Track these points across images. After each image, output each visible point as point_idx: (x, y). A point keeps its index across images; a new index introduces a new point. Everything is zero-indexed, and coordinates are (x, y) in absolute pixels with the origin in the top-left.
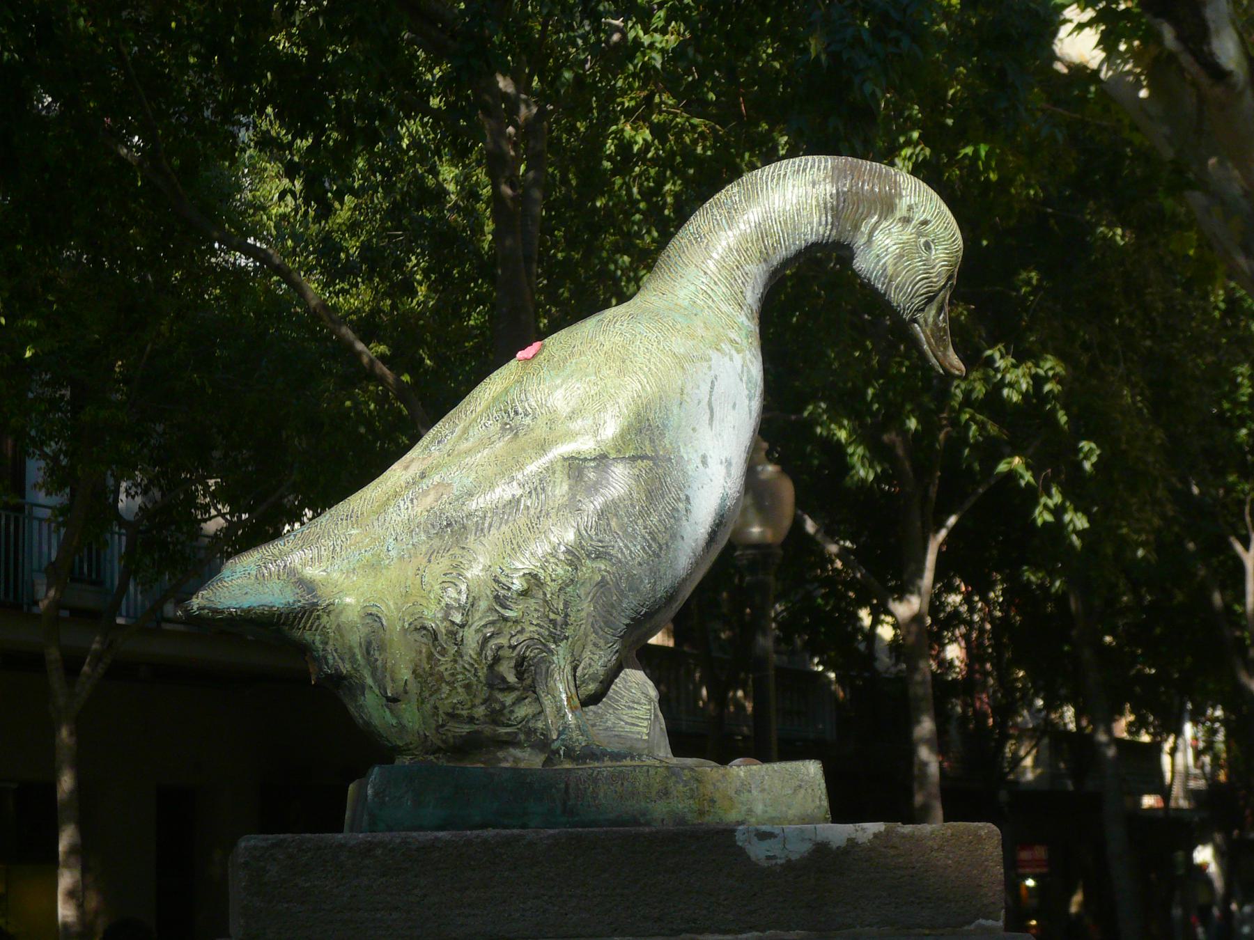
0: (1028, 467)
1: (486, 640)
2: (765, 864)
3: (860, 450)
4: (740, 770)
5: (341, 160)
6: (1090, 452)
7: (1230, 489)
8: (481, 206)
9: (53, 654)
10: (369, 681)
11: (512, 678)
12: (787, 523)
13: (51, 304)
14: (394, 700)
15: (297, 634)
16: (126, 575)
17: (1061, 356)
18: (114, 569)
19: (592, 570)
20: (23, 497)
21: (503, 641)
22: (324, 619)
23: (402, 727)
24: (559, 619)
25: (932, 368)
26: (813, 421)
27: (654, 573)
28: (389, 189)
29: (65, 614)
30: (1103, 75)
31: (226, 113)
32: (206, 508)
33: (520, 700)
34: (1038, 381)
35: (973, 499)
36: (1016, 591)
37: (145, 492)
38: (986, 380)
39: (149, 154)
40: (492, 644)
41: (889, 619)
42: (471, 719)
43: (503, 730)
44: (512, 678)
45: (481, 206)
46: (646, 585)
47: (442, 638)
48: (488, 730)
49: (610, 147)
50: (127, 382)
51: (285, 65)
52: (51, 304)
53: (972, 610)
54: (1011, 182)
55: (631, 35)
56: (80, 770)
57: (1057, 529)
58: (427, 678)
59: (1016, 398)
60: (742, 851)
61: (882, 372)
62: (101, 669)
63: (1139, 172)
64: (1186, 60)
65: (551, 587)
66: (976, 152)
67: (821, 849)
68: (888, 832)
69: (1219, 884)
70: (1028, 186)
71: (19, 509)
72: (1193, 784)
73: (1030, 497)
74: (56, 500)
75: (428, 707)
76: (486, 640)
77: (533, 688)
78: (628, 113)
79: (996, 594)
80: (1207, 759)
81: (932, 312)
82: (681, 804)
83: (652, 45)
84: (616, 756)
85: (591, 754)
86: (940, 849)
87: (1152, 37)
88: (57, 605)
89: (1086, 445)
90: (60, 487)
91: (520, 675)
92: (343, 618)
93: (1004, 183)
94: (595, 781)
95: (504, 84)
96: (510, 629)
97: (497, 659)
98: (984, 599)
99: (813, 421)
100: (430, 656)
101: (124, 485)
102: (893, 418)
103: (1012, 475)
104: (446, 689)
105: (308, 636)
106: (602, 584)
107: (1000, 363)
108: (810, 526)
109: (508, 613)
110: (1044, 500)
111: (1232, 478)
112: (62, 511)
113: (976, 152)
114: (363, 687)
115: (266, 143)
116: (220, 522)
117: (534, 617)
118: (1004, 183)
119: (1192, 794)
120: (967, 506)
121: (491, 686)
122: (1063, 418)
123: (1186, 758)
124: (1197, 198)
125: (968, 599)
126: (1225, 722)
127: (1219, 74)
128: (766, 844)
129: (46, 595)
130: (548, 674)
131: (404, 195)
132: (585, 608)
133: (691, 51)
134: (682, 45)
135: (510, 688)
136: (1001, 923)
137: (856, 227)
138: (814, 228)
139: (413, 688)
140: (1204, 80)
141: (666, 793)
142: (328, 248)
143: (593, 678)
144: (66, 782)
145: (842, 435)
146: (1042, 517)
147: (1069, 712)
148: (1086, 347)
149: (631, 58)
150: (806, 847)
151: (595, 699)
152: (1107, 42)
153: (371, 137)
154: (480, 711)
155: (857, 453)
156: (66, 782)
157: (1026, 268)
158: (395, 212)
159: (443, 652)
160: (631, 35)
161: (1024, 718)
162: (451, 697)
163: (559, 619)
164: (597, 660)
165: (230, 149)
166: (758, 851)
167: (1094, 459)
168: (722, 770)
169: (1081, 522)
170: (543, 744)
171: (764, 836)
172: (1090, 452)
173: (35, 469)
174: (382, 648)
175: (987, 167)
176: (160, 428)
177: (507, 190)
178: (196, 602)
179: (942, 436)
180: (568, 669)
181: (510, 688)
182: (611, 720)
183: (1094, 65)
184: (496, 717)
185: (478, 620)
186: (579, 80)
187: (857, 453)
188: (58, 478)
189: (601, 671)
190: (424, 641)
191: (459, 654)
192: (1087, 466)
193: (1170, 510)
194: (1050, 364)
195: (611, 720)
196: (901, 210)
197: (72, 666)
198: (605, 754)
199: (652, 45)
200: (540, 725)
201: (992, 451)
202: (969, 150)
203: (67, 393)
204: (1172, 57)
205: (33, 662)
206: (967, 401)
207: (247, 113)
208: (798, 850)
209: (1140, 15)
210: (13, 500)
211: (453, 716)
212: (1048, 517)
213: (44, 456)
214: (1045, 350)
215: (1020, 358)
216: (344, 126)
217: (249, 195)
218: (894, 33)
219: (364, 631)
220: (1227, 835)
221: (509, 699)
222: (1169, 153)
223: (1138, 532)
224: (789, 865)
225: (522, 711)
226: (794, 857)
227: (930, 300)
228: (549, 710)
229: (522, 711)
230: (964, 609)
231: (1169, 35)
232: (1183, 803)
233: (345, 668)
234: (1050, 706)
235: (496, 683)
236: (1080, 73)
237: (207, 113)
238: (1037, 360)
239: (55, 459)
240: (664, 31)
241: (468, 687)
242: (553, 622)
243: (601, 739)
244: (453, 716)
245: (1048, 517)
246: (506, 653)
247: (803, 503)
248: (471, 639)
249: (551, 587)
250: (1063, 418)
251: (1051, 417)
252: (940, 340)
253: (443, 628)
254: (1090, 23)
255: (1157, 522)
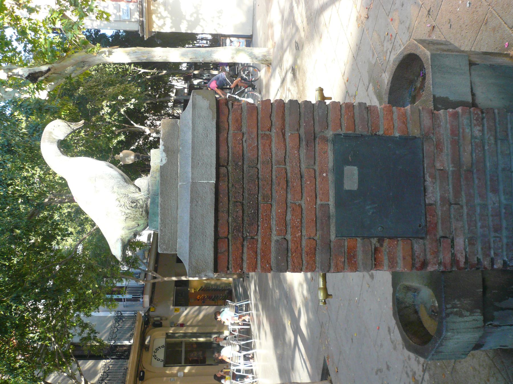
0: (123, 108)
1: (128, 208)
2: (166, 161)
3: (119, 138)
4: (152, 164)
5: (61, 230)
6: (120, 97)
8: (71, 205)
9: (152, 281)
10: (135, 229)
11: (135, 204)
12: (131, 152)
13: (88, 282)
14: (138, 225)
15: (126, 242)
16: (138, 268)
17: (103, 101)
19: (116, 189)
20: (124, 287)
21: (128, 205)
22: (124, 237)
24: (124, 195)
25: (83, 126)
28: (68, 222)
29: (145, 279)
30: (49, 91)
31: (52, 251)
33: (139, 203)
34: (107, 106)
35: (128, 118)
36: (148, 111)
37: (123, 265)
38: (106, 115)
39: (60, 264)
40: (128, 207)
41: (152, 134)
42: (142, 211)
43: (144, 206)
44: (135, 204)
45: (71, 205)
46: (119, 180)
47: (127, 216)
48: (144, 208)
49: (60, 181)
51: (43, 240)
52: (88, 282)
53: (151, 120)
54: (69, 109)
55: (37, 177)
56: (171, 276)
57: (134, 105)
58: (135, 219)
59: (110, 110)
60: (164, 165)
61: (104, 133)
63: (69, 85)
64: (46, 75)
65: (119, 197)
66: (63, 114)
68: (162, 139)
70: (70, 105)
71: (126, 287)
74: (124, 280)
75: (140, 219)
76: (128, 208)
77: (137, 200)
78: (54, 178)
80: (179, 81)
83: (39, 173)
85: (148, 190)
86: (165, 130)
87: (42, 82)
88: (143, 280)
89: (119, 98)
91: (135, 203)
92: (124, 234)
93: (69, 110)
94: (153, 190)
95: (46, 200)
96: (126, 204)
97: (131, 207)
98: (149, 117)
100: (130, 218)
101: (122, 269)
102: (113, 132)
103: (124, 111)
104: (136, 216)
105: (127, 240)
106: (118, 187)
107: (103, 112)
108: (132, 148)
109: (123, 205)
110: (129, 106)
111: (128, 73)
112: (127, 280)
113: (63, 114)
115: (58, 243)
117: (124, 200)
118: (69, 110)
119: (185, 83)
120: (130, 120)
121: (136, 208)
122: (114, 102)
123: (178, 84)
124: (73, 76)
125: (149, 120)
126: (172, 77)
127: (49, 70)
128: (163, 160)
129: (142, 283)
131: (69, 219)
132: (123, 191)
133: (40, 166)
134: (39, 167)
135: (137, 204)
136: (178, 120)
137: (55, 139)
138: (55, 147)
139: (136, 221)
140: (50, 72)
142: (79, 233)
143: (136, 189)
144: (174, 279)
145: (116, 141)
146: (132, 107)
147: (169, 104)
149: (41, 177)
150: (164, 153)
151: (139, 189)
152: (42, 89)
153: (58, 224)
154: (141, 210)
155: (119, 139)
156: (174, 279)
158: (72, 220)
159: (130, 216)
160: (37, 177)
162: (138, 215)
163: (124, 195)
164: (132, 188)
165: (59, 250)
166: (164, 162)
167: (122, 97)
168: (152, 167)
169: (133, 100)
170: (147, 199)
171: (161, 161)
172: (120, 97)
173: (119, 284)
175: (66, 113)
176: (112, 263)
179: (117, 123)
180: (134, 194)
181: (137, 204)
182: (143, 187)
183: (47, 92)
186: (46, 187)
187: (119, 139)
188: (121, 280)
189: (135, 188)
190: (128, 220)
192: (123, 98)
194: (104, 103)
195: (143, 187)
196: (52, 131)
197: (155, 278)
198: (148, 188)
199: (39, 173)
200: (144, 199)
201: (120, 115)
202: (63, 116)
203: (105, 279)
205: (154, 285)
206: (110, 119)
207: (52, 247)
208: (164, 155)
209: (37, 83)
210: (124, 289)
211: (141, 215)
212: (132, 105)
215: (102, 109)
216: (55, 229)
217: (69, 247)
218: (38, 129)
219: (126, 230)
220: (192, 78)
221: (139, 205)
222: (64, 80)
223: (135, 90)
224: (167, 156)
225: (141, 202)
227: (69, 126)
228: (141, 198)
229: (141, 202)
230: (150, 121)
231: (40, 78)
232: (187, 85)
233: (133, 233)
234: (169, 107)
235: (136, 207)
236: (49, 94)
237: (52, 254)
238: (103, 106)
240: (36, 171)
241: (136, 212)
242: (125, 196)
243: (146, 188)
244: (141, 215)
245: (132, 105)
247: (128, 149)
248: (128, 211)
249: (119, 197)
250: (114, 102)
252: (77, 125)
253: (125, 216)
254: (39, 92)
255: (133, 87)
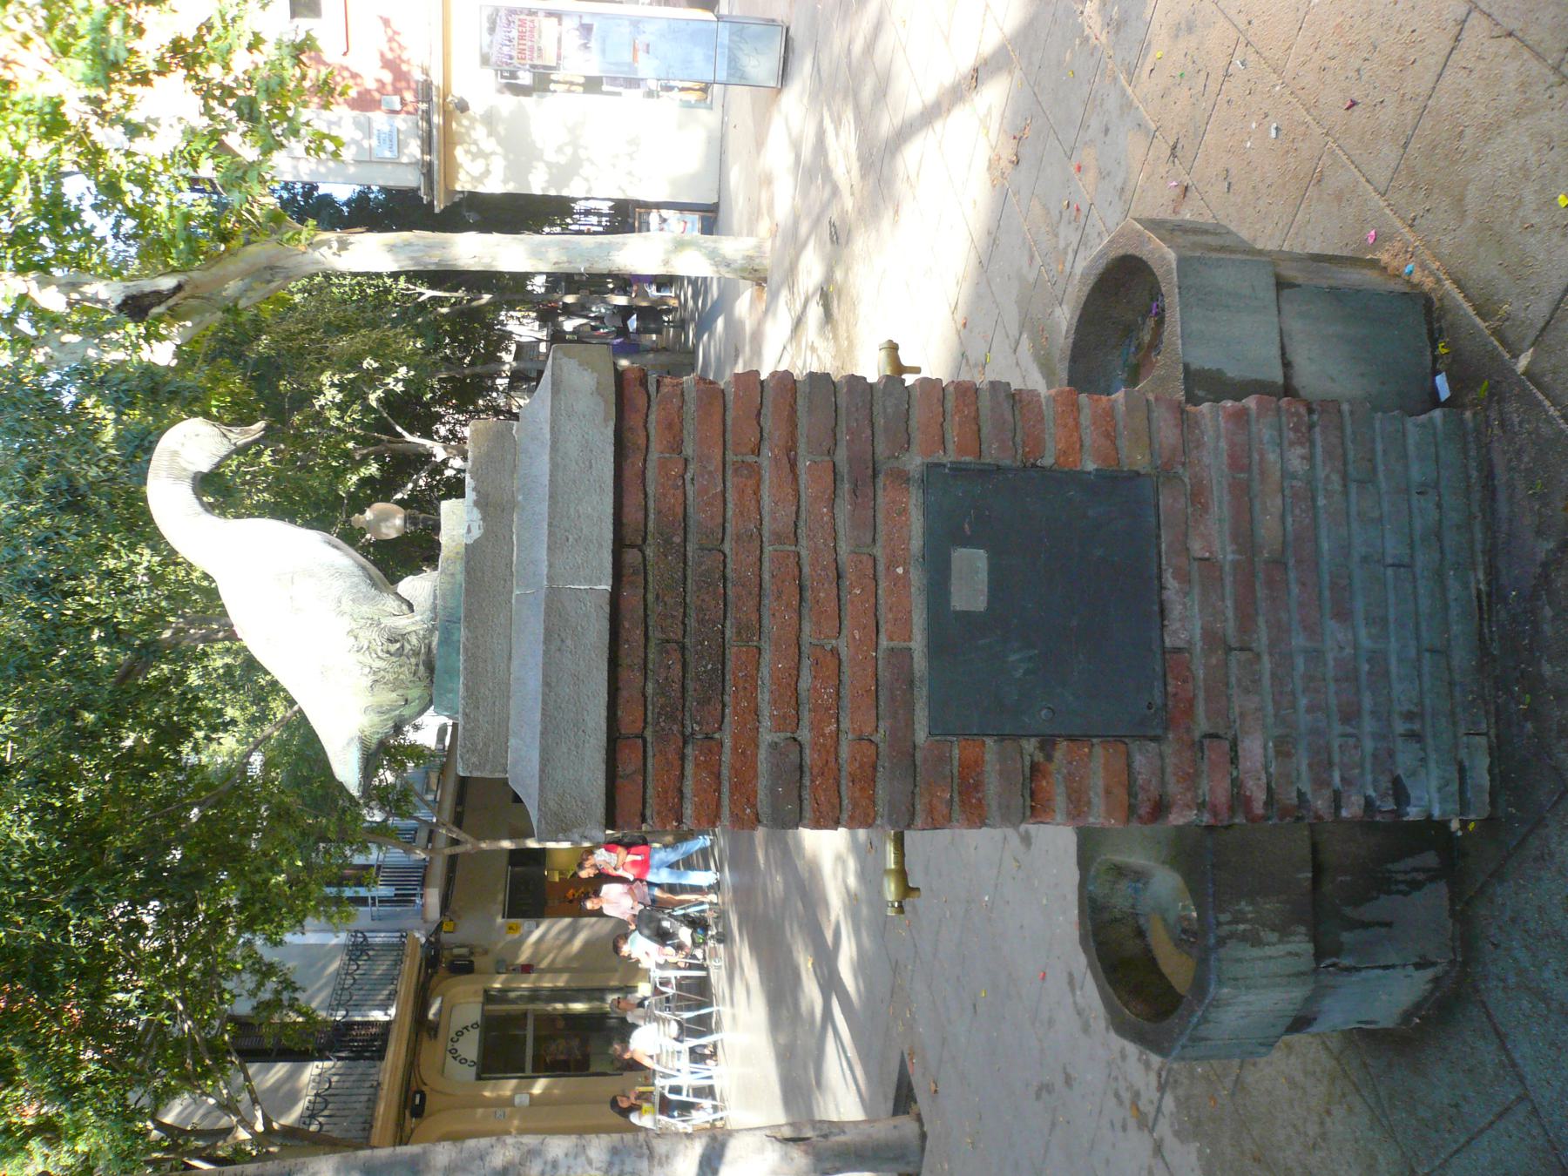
3: (363, 470)
4: (444, 538)
5: (205, 713)
7: (396, 299)
8: (234, 647)
9: (448, 851)
11: (398, 645)
14: (406, 701)
15: (373, 747)
17: (322, 372)
18: (411, 823)
19: (347, 605)
20: (372, 866)
23: (419, 698)
26: (348, 493)
27: (350, 575)
29: (430, 846)
32: (381, 781)
33: (409, 642)
34: (333, 385)
36: (441, 401)
38: (330, 409)
40: (380, 654)
42: (417, 665)
44: (398, 645)
46: (356, 580)
48: (422, 657)
50: (317, 817)
58: (396, 685)
59: (340, 396)
61: (325, 458)
62: (455, 829)
64: (171, 302)
65: (354, 625)
66: (215, 406)
67: (477, 504)
69: (584, 321)
70: (234, 383)
71: (379, 867)
72: (537, 328)
73: (389, 393)
74: (373, 848)
75: (410, 685)
77: (403, 635)
79: (441, 410)
81: (230, 435)
82: (459, 567)
84: (435, 597)
88: (425, 849)
89: (365, 365)
90: (367, 847)
91: (397, 641)
93: (231, 393)
99: (348, 493)
102: (347, 455)
103: (379, 400)
104: (402, 677)
105: (374, 741)
106: (353, 600)
110: (391, 386)
112: (380, 847)
113: (215, 406)
114: (400, 716)
116: (388, 773)
119: (541, 327)
122: (351, 376)
124: (242, 304)
125: (444, 424)
129: (420, 855)
130: (395, 628)
132: (366, 610)
134: (148, 546)
135: (403, 646)
137: (185, 470)
139: (400, 692)
140: (181, 294)
141: (453, 575)
143: (400, 606)
144: (506, 844)
146: (400, 388)
147: (499, 381)
148: (319, 361)
151: (410, 607)
154: (413, 660)
155: (364, 472)
157: (277, 387)
159: (384, 677)
161: (502, 402)
162: (406, 674)
164: (391, 604)
166: (477, 533)
168: (443, 548)
170: (431, 631)
172: (369, 363)
173: (358, 859)
174: (381, 706)
175: (224, 402)
176: (341, 802)
177: (221, 635)
178: (355, 793)
181: (403, 646)
184: (416, 653)
185: (367, 659)
186: (168, 598)
187: (364, 472)
188: (364, 849)
189: (397, 603)
190: (378, 686)
191: (384, 670)
193: (400, 330)
194: (325, 378)
195: (421, 599)
197: (455, 842)
201: (367, 409)
204: (169, 309)
205: (452, 861)
206: (341, 418)
207: (181, 759)
210: (374, 870)
211: (415, 674)
212: (401, 384)
213: (352, 856)
214: (317, 380)
215: (320, 392)
221: (407, 647)
222: (220, 314)
224: (484, 519)
225: (414, 641)
226: (480, 516)
227: (225, 436)
229: (414, 641)
230: (448, 427)
232: (545, 333)
233: (391, 724)
234: (497, 390)
238: (322, 384)
239: (354, 851)
240: (141, 555)
241: (401, 666)
243: (428, 604)
244: (415, 674)
245: (401, 384)
246: (385, 648)
247: (387, 499)
249: (354, 625)
250: (351, 376)
251: (352, 381)
253: (372, 677)
